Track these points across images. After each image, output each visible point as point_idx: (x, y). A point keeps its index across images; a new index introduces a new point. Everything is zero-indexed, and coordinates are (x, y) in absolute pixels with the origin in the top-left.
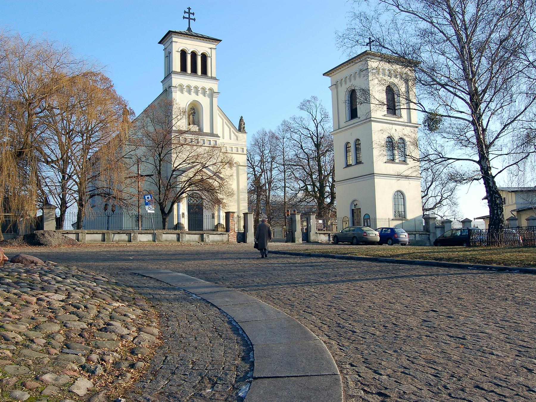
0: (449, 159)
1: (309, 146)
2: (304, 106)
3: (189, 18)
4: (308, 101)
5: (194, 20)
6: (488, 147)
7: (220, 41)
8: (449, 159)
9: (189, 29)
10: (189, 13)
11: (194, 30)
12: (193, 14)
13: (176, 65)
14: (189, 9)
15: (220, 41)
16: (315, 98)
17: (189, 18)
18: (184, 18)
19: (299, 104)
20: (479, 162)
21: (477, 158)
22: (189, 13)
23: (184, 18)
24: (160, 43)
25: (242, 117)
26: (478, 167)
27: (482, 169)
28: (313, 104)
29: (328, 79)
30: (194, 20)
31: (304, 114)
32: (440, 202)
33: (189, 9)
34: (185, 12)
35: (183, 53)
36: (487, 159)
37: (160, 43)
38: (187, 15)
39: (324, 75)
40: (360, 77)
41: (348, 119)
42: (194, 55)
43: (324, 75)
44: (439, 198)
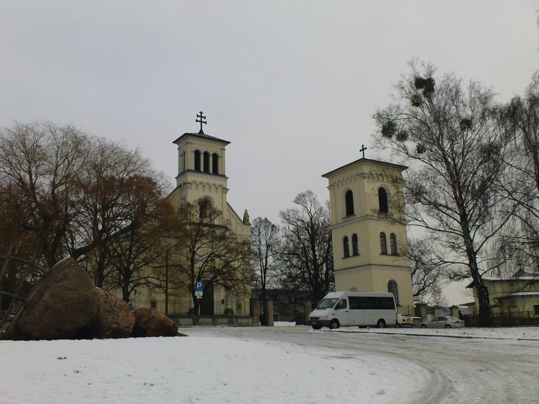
0: (447, 262)
1: (305, 235)
2: (300, 199)
3: (201, 122)
4: (304, 196)
5: (206, 123)
6: (475, 253)
7: (230, 143)
8: (447, 262)
9: (201, 131)
10: (201, 117)
11: (206, 132)
12: (205, 118)
13: (191, 165)
14: (201, 113)
15: (230, 143)
16: (310, 193)
17: (201, 122)
18: (197, 121)
19: (294, 199)
20: (469, 265)
21: (467, 262)
22: (201, 117)
23: (197, 121)
24: (174, 142)
25: (246, 211)
26: (468, 268)
27: (472, 269)
28: (308, 198)
29: (326, 180)
30: (198, 116)
31: (299, 207)
32: (423, 289)
33: (363, 146)
34: (198, 116)
35: (197, 153)
36: (475, 263)
37: (174, 142)
38: (199, 119)
39: (322, 176)
40: (355, 180)
41: (345, 215)
42: (206, 154)
43: (322, 176)
44: (421, 286)
